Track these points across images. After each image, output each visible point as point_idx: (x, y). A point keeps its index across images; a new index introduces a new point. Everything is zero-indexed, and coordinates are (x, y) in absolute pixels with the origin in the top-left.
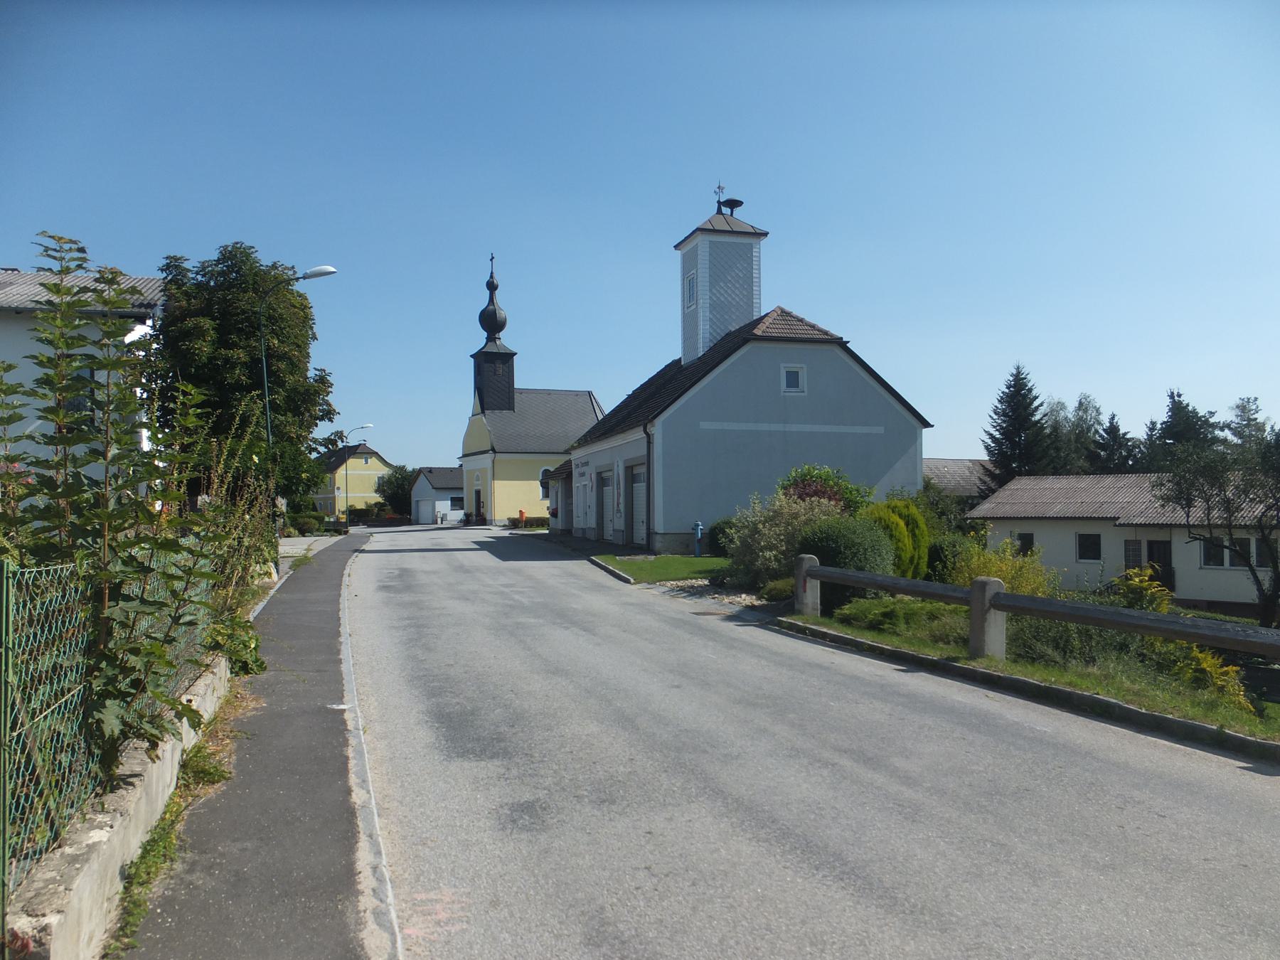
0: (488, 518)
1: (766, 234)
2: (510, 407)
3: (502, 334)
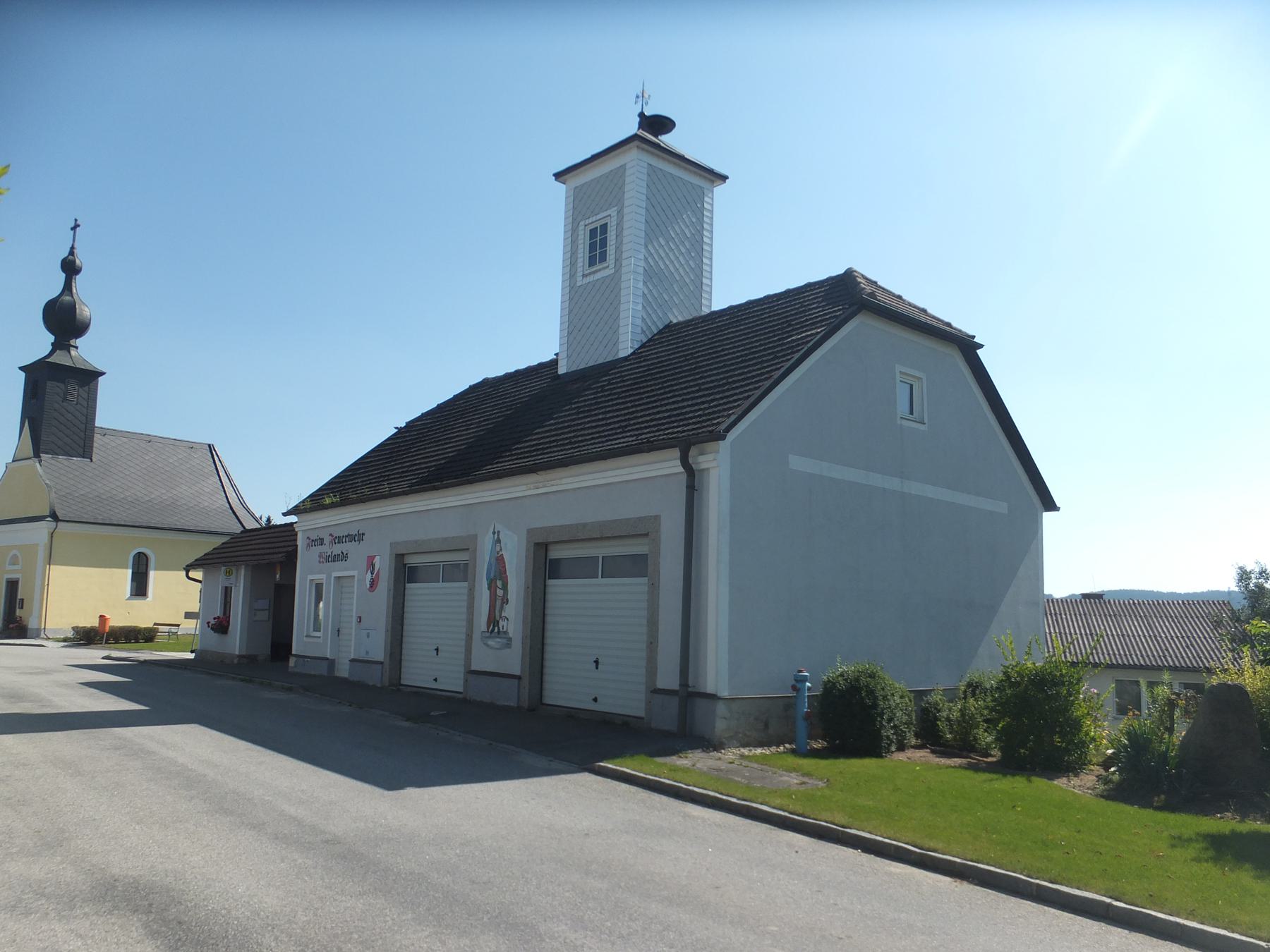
0: (32, 624)
1: (724, 178)
2: (85, 451)
3: (79, 342)
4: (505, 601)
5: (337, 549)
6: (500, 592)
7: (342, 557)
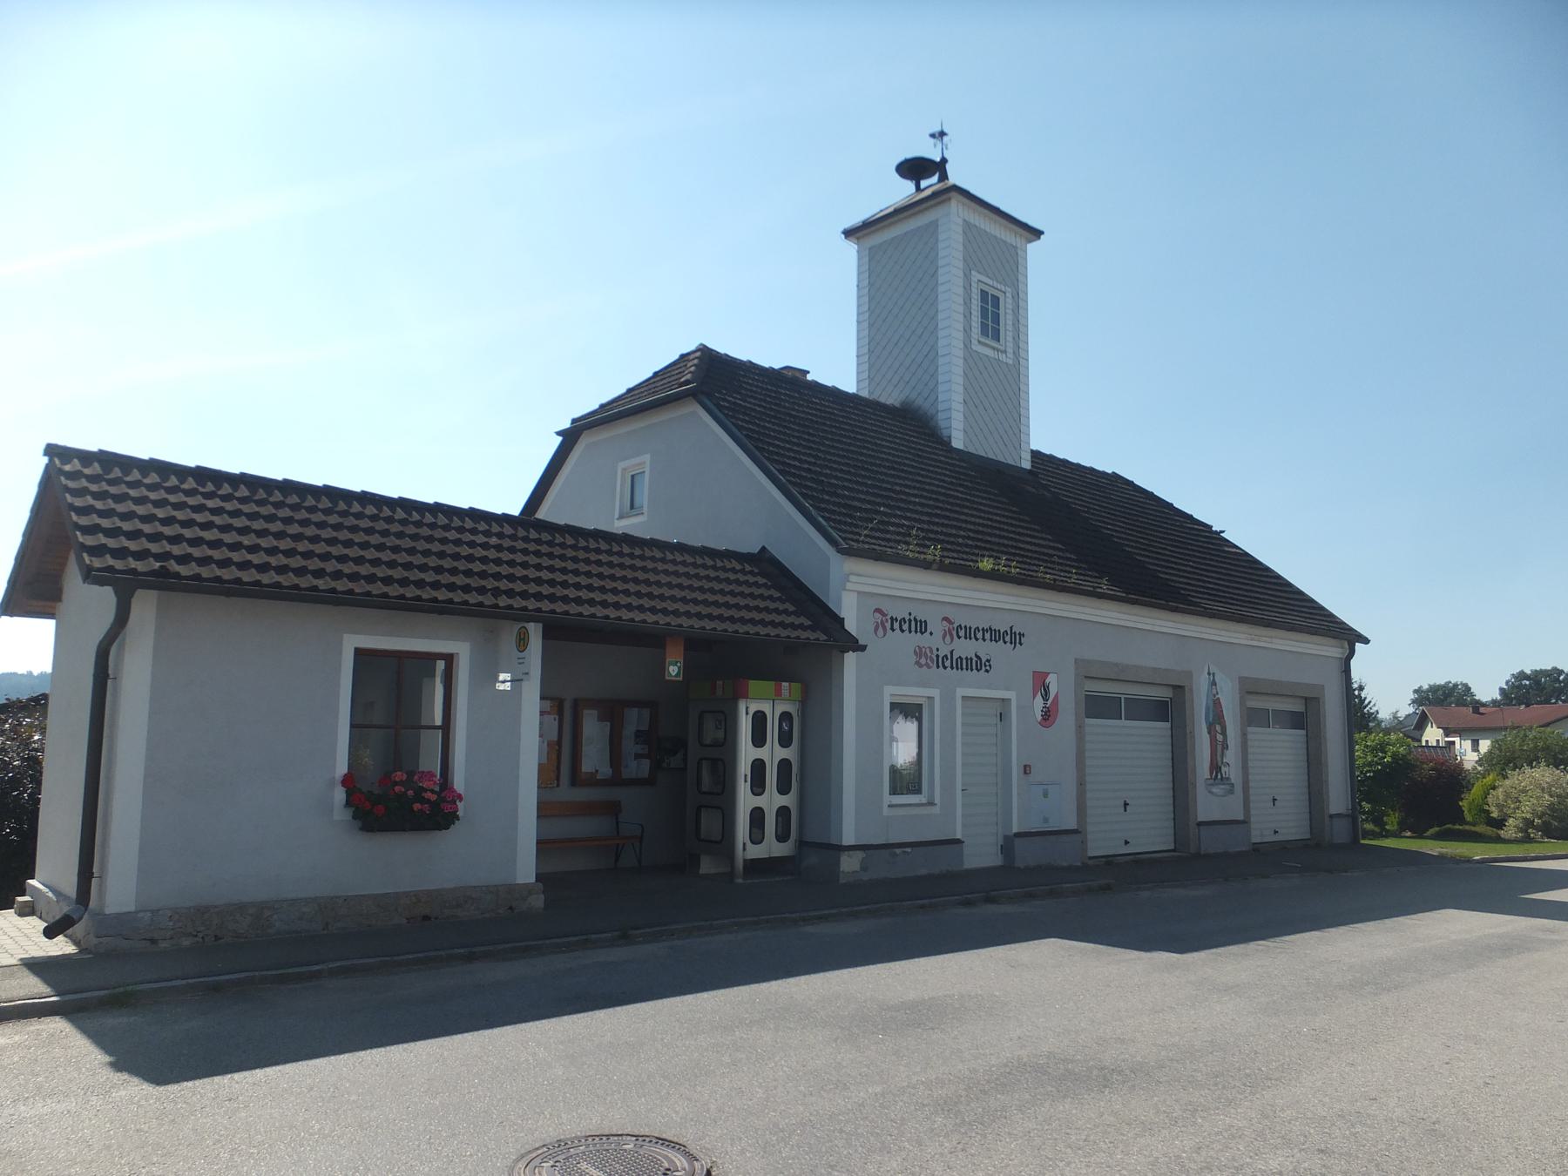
1: (1037, 234)
4: (1225, 746)
5: (965, 648)
6: (1220, 738)
7: (979, 664)
